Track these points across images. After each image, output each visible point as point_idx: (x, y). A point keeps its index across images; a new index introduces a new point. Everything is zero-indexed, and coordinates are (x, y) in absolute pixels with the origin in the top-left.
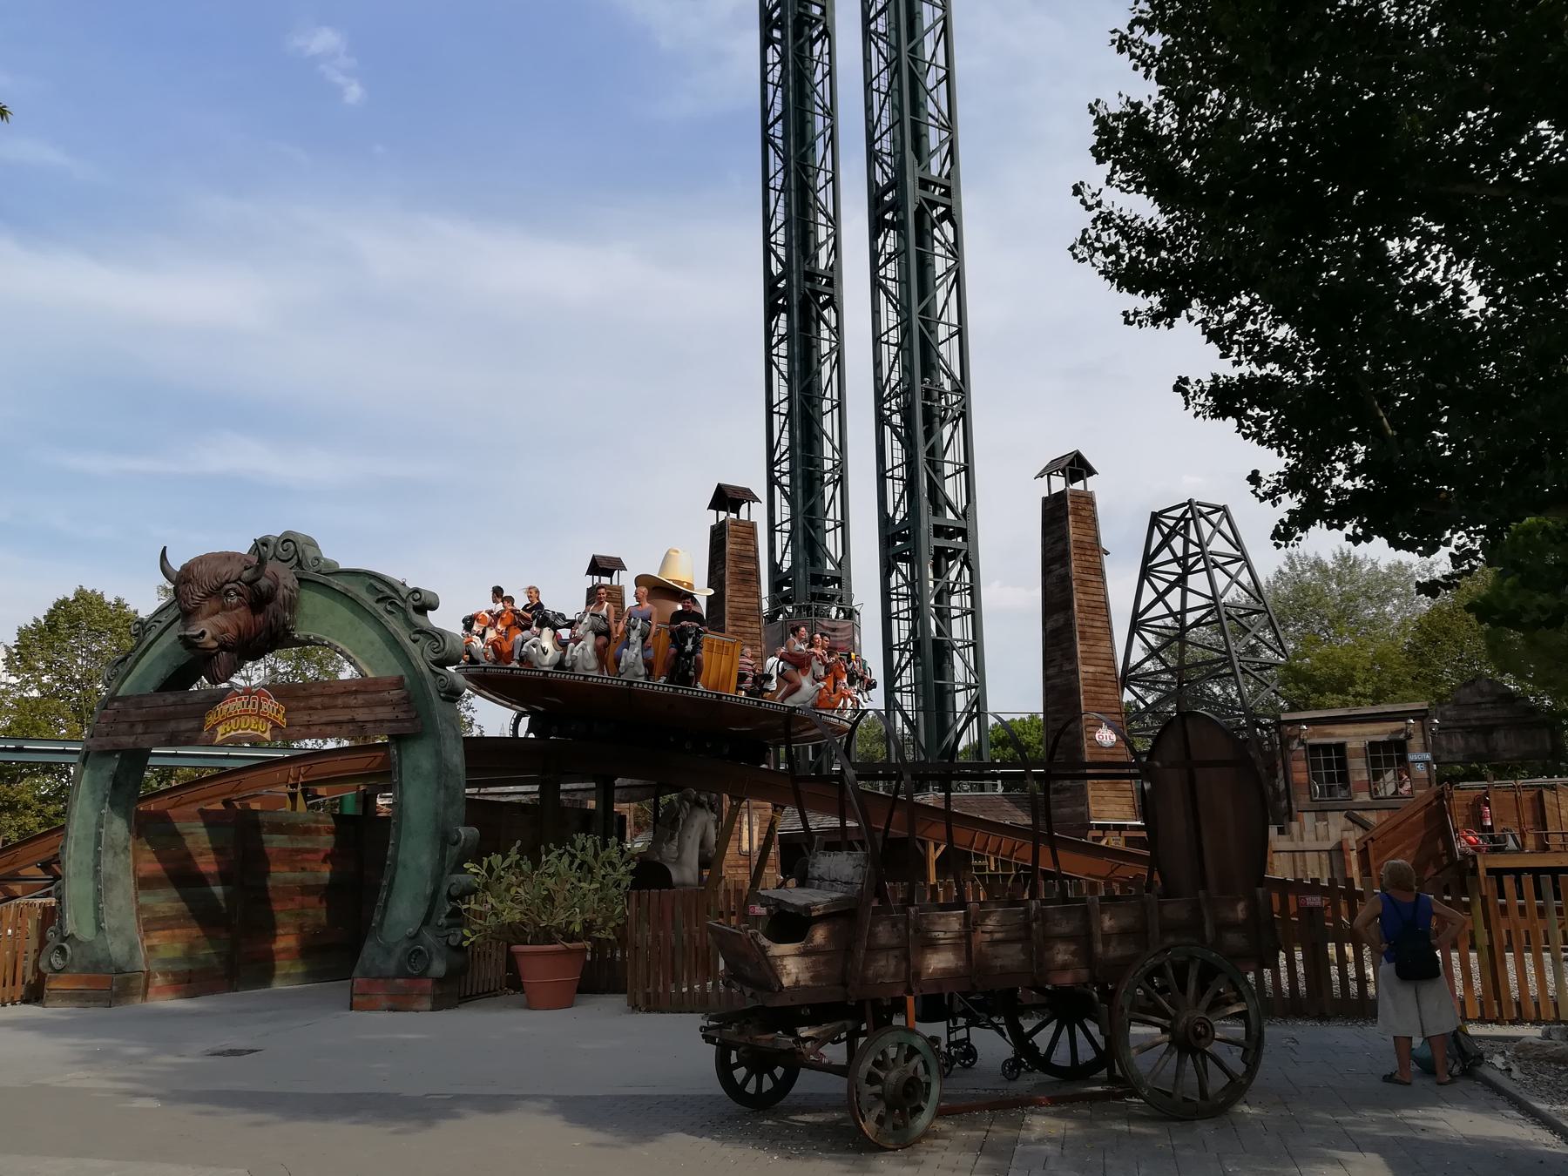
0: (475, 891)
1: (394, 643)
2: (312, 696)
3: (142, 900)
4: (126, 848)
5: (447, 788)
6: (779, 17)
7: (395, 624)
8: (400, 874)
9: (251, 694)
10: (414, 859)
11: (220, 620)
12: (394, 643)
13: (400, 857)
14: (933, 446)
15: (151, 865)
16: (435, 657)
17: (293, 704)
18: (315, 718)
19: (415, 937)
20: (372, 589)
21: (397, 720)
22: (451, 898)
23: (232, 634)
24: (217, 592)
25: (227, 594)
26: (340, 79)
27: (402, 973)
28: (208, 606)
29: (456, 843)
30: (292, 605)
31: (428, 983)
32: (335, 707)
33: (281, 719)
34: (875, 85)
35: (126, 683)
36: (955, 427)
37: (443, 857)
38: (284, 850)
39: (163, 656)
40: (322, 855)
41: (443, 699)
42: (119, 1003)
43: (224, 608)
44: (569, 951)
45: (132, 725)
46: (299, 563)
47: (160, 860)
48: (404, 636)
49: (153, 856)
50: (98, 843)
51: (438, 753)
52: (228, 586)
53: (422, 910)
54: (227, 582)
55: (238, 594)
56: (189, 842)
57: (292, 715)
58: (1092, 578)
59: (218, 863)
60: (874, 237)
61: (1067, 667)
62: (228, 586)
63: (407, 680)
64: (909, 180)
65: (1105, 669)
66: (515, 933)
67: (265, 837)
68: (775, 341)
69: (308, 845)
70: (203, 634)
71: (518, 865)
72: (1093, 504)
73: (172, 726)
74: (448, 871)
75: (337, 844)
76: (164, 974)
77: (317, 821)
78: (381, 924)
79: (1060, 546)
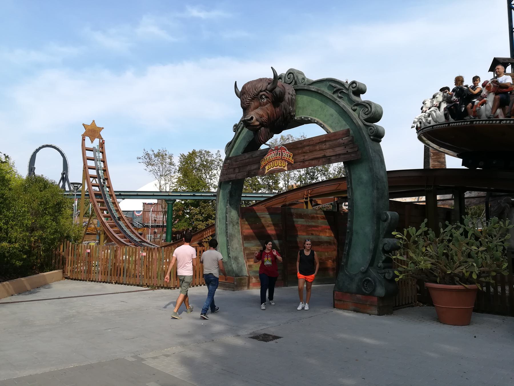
0: (398, 248)
1: (343, 113)
2: (304, 147)
3: (246, 245)
4: (237, 223)
5: (378, 189)
7: (343, 103)
8: (355, 237)
9: (278, 149)
10: (363, 229)
11: (259, 111)
12: (343, 113)
13: (354, 228)
15: (248, 231)
16: (366, 117)
17: (296, 152)
19: (365, 272)
20: (331, 87)
22: (385, 251)
23: (265, 118)
24: (257, 97)
25: (261, 97)
27: (359, 291)
28: (253, 104)
29: (385, 221)
30: (292, 103)
31: (375, 299)
32: (315, 150)
33: (291, 160)
35: (232, 152)
37: (378, 229)
38: (304, 226)
39: (244, 138)
41: (373, 140)
42: (237, 289)
43: (261, 105)
44: (467, 290)
45: (234, 169)
47: (252, 228)
48: (349, 108)
49: (249, 227)
50: (226, 221)
51: (371, 170)
52: (261, 94)
53: (369, 258)
54: (261, 91)
55: (267, 97)
56: (263, 220)
57: (295, 157)
59: (276, 230)
62: (261, 94)
63: (351, 132)
66: (429, 275)
67: (295, 219)
69: (313, 224)
70: (252, 118)
71: (426, 233)
73: (248, 168)
74: (382, 236)
76: (255, 277)
77: (317, 214)
78: (346, 263)
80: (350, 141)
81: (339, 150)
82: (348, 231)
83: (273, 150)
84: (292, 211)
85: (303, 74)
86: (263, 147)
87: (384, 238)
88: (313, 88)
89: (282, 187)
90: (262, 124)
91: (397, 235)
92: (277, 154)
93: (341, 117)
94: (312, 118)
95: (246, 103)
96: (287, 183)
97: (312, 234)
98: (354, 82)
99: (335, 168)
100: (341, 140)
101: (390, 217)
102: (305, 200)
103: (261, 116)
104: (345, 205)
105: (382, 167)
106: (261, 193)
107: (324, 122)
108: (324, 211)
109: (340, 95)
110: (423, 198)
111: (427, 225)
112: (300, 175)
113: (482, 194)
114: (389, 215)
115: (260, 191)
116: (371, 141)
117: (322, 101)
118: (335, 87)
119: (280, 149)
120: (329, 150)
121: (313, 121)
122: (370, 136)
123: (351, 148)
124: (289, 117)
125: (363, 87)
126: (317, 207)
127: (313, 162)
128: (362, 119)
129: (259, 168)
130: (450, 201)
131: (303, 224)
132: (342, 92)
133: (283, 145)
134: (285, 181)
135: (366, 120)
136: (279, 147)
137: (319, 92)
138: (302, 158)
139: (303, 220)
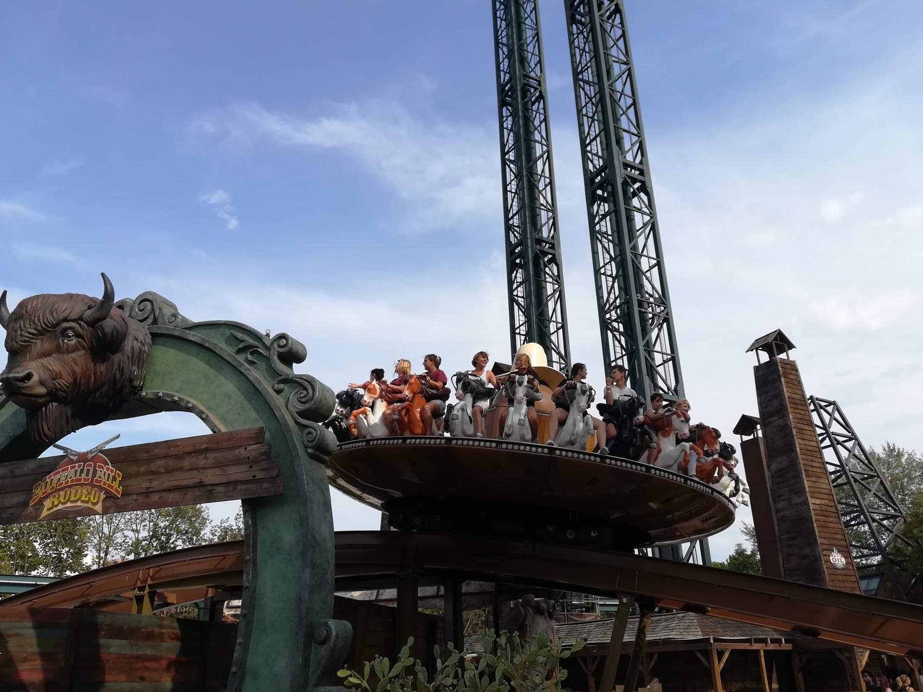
5: (313, 566)
6: (510, 89)
11: (53, 363)
12: (255, 394)
14: (647, 342)
16: (301, 407)
18: (156, 484)
21: (254, 480)
23: (66, 380)
25: (64, 333)
26: (226, 216)
28: (40, 345)
29: (323, 643)
30: (140, 359)
32: (181, 469)
33: (117, 489)
34: (584, 111)
36: (660, 330)
37: (306, 663)
40: (164, 663)
41: (312, 456)
43: (58, 350)
46: (155, 321)
48: (267, 385)
51: (303, 521)
52: (65, 325)
55: (78, 335)
56: (12, 644)
58: (806, 427)
59: (45, 671)
60: (590, 204)
61: (796, 500)
62: (65, 325)
63: (267, 435)
64: (616, 163)
65: (827, 502)
67: (102, 641)
68: (515, 286)
69: (149, 652)
70: (29, 376)
72: (797, 371)
75: (182, 651)
79: (776, 402)
80: (263, 454)
81: (236, 473)
82: (234, 669)
83: (72, 462)
84: (100, 619)
85: (176, 309)
86: (51, 452)
87: (317, 685)
88: (193, 336)
89: (90, 563)
90: (53, 395)
91: (352, 679)
92: (82, 471)
93: (250, 402)
94: (182, 396)
95: (19, 339)
96: (102, 555)
97: (142, 679)
98: (282, 336)
99: (224, 515)
100: (242, 450)
101: (334, 633)
102: (137, 592)
103: (55, 376)
104: (228, 607)
105: (325, 518)
106: (35, 576)
107: (209, 408)
108: (179, 620)
109: (250, 357)
110: (390, 593)
111: (413, 653)
112: (137, 539)
113: (488, 586)
114: (333, 627)
115: (34, 573)
116: (308, 458)
117: (209, 364)
118: (242, 341)
119: (92, 459)
120: (211, 472)
121: (183, 404)
122: (306, 447)
123: (263, 470)
124: (127, 390)
125: (300, 350)
126: (165, 610)
127: (171, 496)
128: (293, 410)
129: (26, 504)
130: (433, 601)
131: (124, 652)
132: (255, 353)
133: (101, 451)
134: (99, 551)
135: (302, 414)
136: (90, 456)
137: (207, 345)
138: (146, 485)
139: (123, 642)
